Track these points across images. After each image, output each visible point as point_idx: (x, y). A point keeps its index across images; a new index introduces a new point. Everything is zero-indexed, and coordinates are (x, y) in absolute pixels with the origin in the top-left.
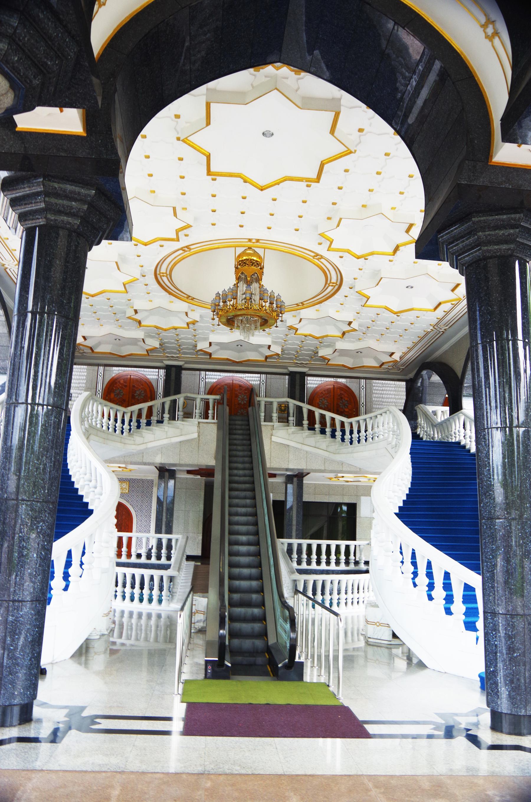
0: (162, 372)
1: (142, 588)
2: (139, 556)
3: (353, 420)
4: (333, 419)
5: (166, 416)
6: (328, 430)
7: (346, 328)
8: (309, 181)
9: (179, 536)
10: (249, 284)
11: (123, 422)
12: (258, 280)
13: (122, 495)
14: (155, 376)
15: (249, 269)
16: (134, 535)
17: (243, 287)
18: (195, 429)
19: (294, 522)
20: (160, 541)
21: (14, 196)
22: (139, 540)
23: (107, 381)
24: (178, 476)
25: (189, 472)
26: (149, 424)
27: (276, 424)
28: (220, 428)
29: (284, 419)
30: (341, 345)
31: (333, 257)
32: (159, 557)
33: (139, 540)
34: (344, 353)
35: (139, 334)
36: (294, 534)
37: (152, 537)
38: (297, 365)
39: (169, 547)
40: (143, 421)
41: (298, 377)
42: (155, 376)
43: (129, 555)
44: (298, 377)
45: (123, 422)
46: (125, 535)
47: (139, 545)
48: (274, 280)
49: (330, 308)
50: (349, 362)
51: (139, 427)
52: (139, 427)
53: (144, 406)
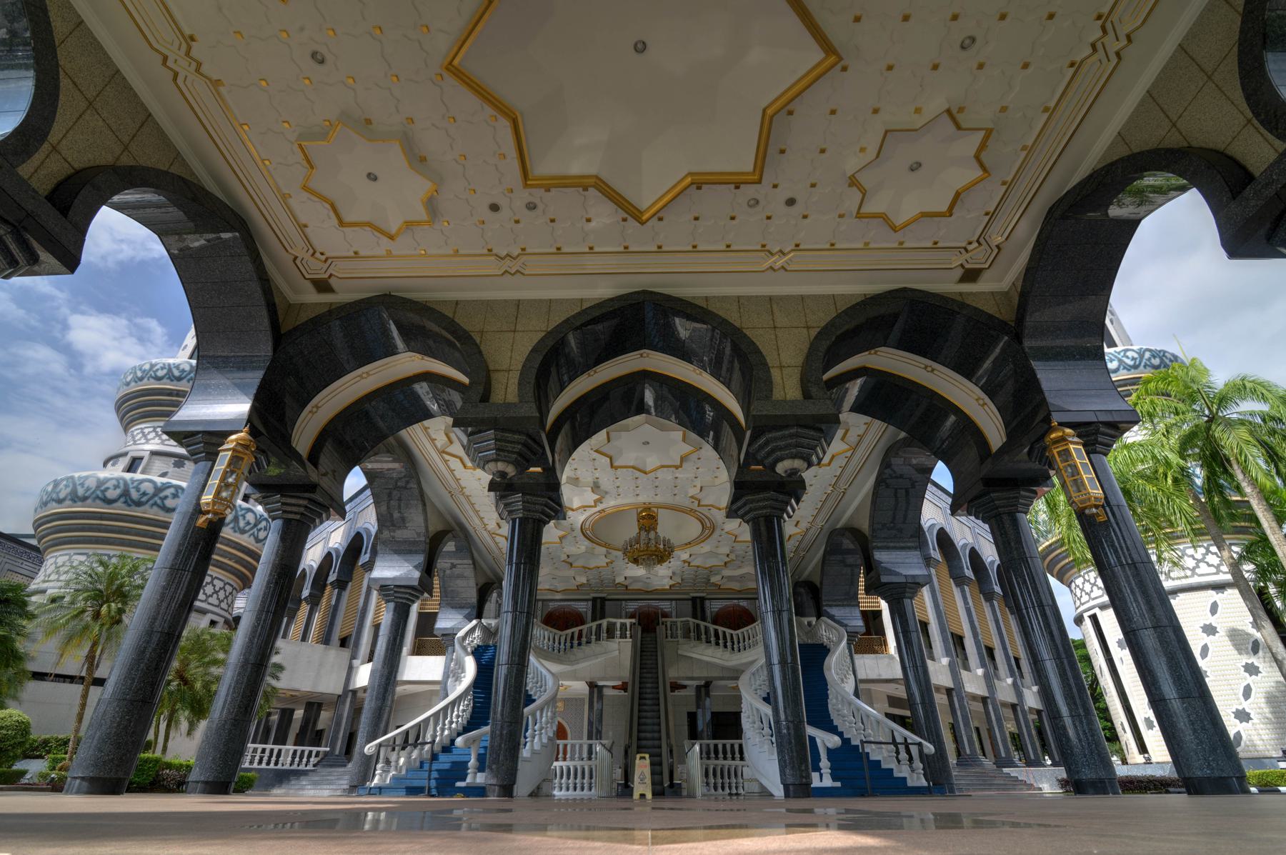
0: (590, 603)
3: (739, 632)
8: (677, 467)
10: (648, 531)
12: (654, 529)
14: (584, 608)
15: (648, 519)
16: (569, 742)
17: (643, 534)
22: (573, 746)
23: (545, 613)
26: (580, 644)
27: (681, 640)
28: (634, 646)
29: (686, 635)
31: (704, 510)
33: (573, 746)
34: (730, 578)
40: (576, 642)
42: (584, 608)
48: (667, 527)
49: (706, 548)
50: (736, 586)
53: (576, 630)
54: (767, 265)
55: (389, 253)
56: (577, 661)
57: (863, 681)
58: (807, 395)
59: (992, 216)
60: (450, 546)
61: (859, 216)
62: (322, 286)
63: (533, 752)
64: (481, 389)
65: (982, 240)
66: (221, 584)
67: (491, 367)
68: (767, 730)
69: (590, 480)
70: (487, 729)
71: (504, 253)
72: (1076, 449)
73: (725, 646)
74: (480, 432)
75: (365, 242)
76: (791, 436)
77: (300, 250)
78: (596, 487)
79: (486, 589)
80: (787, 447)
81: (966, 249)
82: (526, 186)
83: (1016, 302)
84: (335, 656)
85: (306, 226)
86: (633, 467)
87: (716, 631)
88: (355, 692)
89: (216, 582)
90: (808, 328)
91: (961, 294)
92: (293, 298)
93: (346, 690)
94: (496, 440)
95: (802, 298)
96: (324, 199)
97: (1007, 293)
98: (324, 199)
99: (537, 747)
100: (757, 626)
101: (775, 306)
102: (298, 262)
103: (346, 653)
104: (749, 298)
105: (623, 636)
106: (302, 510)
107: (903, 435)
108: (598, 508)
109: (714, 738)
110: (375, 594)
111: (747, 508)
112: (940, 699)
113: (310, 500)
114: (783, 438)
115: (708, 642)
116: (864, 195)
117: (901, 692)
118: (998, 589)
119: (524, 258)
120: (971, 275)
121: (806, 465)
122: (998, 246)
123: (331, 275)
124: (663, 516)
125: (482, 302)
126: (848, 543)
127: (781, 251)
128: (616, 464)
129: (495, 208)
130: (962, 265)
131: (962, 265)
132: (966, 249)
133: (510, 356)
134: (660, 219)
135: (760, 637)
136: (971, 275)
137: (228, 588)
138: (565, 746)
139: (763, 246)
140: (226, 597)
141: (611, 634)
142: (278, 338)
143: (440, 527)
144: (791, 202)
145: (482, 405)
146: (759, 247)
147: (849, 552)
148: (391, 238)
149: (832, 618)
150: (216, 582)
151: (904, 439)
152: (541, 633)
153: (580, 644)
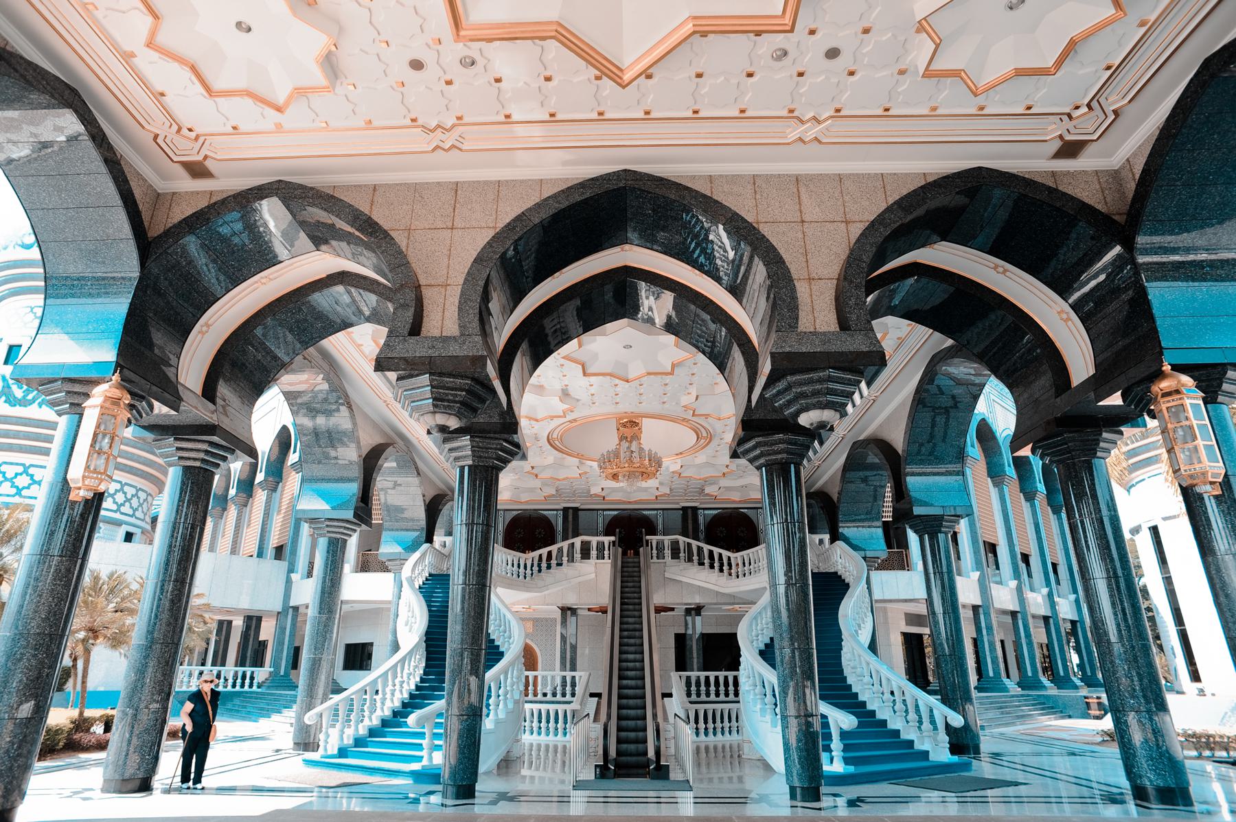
1: (557, 721)
2: (545, 695)
4: (720, 555)
5: (565, 559)
6: (716, 565)
7: (726, 470)
9: (582, 673)
11: (525, 568)
13: (527, 635)
15: (630, 426)
18: (593, 569)
19: (695, 655)
20: (564, 678)
21: (500, 538)
22: (545, 678)
24: (579, 612)
25: (589, 610)
28: (614, 565)
30: (725, 483)
31: (701, 421)
32: (564, 695)
33: (545, 678)
34: (728, 489)
35: (537, 483)
36: (695, 667)
37: (558, 674)
38: (687, 501)
39: (573, 685)
40: (544, 565)
41: (690, 511)
43: (535, 695)
44: (690, 511)
45: (525, 568)
46: (531, 674)
47: (545, 685)
49: (701, 458)
51: (540, 571)
52: (540, 571)
54: (793, 136)
55: (279, 126)
56: (546, 587)
57: (877, 601)
58: (844, 325)
59: (1115, 71)
60: (388, 463)
61: (928, 74)
62: (197, 170)
63: (498, 722)
64: (410, 314)
65: (1094, 104)
66: (133, 491)
67: (423, 282)
68: (769, 698)
69: (558, 386)
70: (439, 705)
71: (434, 124)
72: (1193, 399)
73: (721, 570)
74: (411, 376)
75: (245, 113)
76: (820, 381)
77: (158, 124)
78: (565, 394)
79: (434, 508)
80: (816, 393)
81: (1070, 116)
82: (458, 37)
83: (1130, 195)
84: (273, 569)
85: (162, 95)
86: (610, 375)
87: (711, 552)
88: (296, 609)
89: (126, 488)
90: (847, 222)
91: (1053, 174)
92: (161, 186)
93: (286, 607)
94: (433, 387)
95: (840, 178)
96: (181, 60)
97: (1116, 172)
98: (181, 60)
99: (502, 715)
100: (760, 550)
101: (803, 190)
102: (160, 140)
103: (284, 565)
104: (768, 178)
105: (600, 556)
106: (202, 455)
107: (950, 342)
108: (569, 418)
109: (705, 670)
110: (305, 529)
111: (758, 452)
112: (966, 615)
113: (211, 444)
114: (811, 382)
115: (701, 564)
116: (937, 46)
117: (922, 609)
118: (1041, 487)
119: (460, 129)
120: (1070, 149)
121: (838, 415)
122: (1116, 112)
123: (206, 157)
124: (646, 424)
125: (407, 186)
126: (873, 458)
127: (814, 118)
128: (589, 371)
129: (417, 65)
130: (1061, 137)
131: (1061, 137)
132: (1070, 116)
133: (447, 261)
134: (649, 77)
135: (764, 563)
136: (1070, 149)
137: (142, 495)
138: (536, 677)
139: (791, 111)
140: (141, 505)
141: (586, 554)
142: (146, 245)
143: (378, 440)
144: (833, 53)
145: (413, 340)
146: (785, 113)
147: (873, 467)
148: (279, 109)
149: (847, 541)
150: (126, 488)
151: (951, 347)
152: (501, 557)
153: (549, 567)
